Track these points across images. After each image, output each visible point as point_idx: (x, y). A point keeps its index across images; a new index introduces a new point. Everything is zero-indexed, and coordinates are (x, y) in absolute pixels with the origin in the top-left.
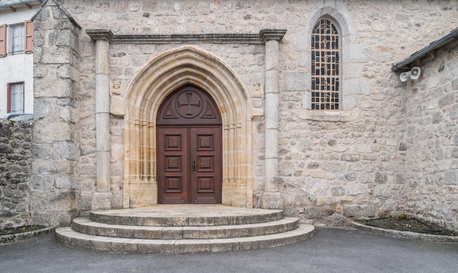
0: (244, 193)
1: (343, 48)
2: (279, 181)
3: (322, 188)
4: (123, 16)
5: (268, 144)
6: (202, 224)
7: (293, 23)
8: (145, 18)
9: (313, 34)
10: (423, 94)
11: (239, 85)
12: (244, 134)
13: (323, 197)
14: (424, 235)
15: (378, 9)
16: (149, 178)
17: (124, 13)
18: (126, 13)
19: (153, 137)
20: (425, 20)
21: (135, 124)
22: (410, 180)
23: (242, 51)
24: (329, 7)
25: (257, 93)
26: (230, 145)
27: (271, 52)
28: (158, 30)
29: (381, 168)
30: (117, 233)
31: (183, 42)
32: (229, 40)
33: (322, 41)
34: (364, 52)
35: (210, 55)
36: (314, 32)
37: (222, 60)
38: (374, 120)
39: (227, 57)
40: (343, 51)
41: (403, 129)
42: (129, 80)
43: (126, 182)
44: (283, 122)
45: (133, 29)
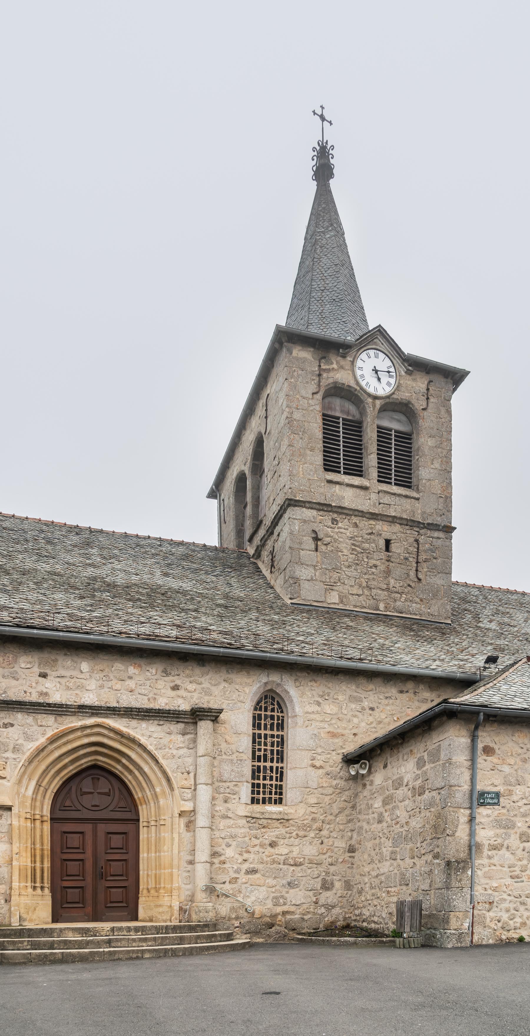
0: (169, 905)
1: (289, 732)
2: (210, 890)
3: (261, 897)
4: (11, 673)
5: (199, 845)
6: (128, 934)
7: (230, 699)
8: (41, 679)
9: (255, 712)
10: (371, 790)
11: (164, 773)
12: (170, 833)
13: (262, 907)
14: (360, 939)
15: (329, 688)
16: (42, 888)
17: (12, 670)
18: (14, 669)
19: (48, 835)
20: (380, 703)
21: (26, 818)
22: (358, 886)
23: (169, 730)
24: (273, 682)
25: (186, 783)
26: (150, 847)
27: (204, 735)
28: (59, 696)
29: (327, 873)
30: (31, 945)
31: (93, 715)
32: (152, 716)
33: (265, 720)
34: (312, 738)
35: (129, 734)
36: (255, 709)
37: (143, 741)
38: (322, 818)
39: (150, 736)
40: (289, 735)
41: (353, 829)
42: (18, 760)
43: (15, 893)
44: (217, 819)
45: (25, 692)
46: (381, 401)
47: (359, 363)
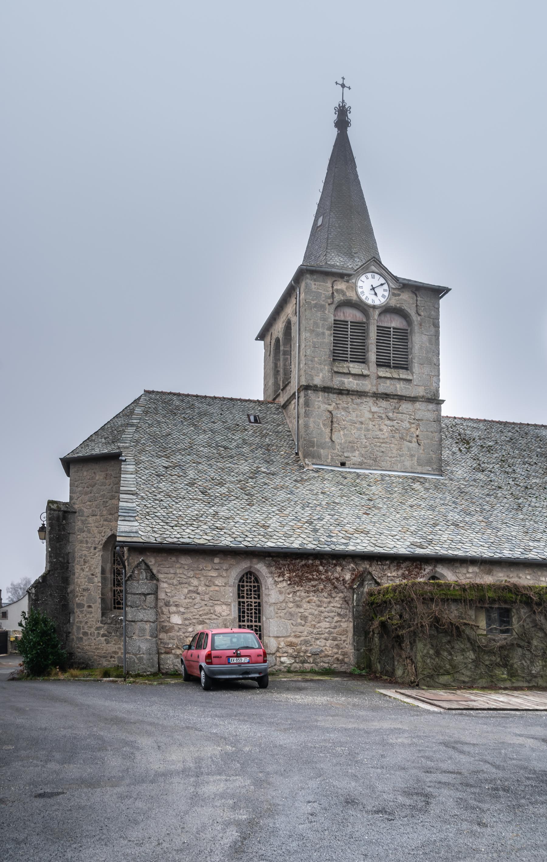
46: (379, 310)
47: (360, 284)
